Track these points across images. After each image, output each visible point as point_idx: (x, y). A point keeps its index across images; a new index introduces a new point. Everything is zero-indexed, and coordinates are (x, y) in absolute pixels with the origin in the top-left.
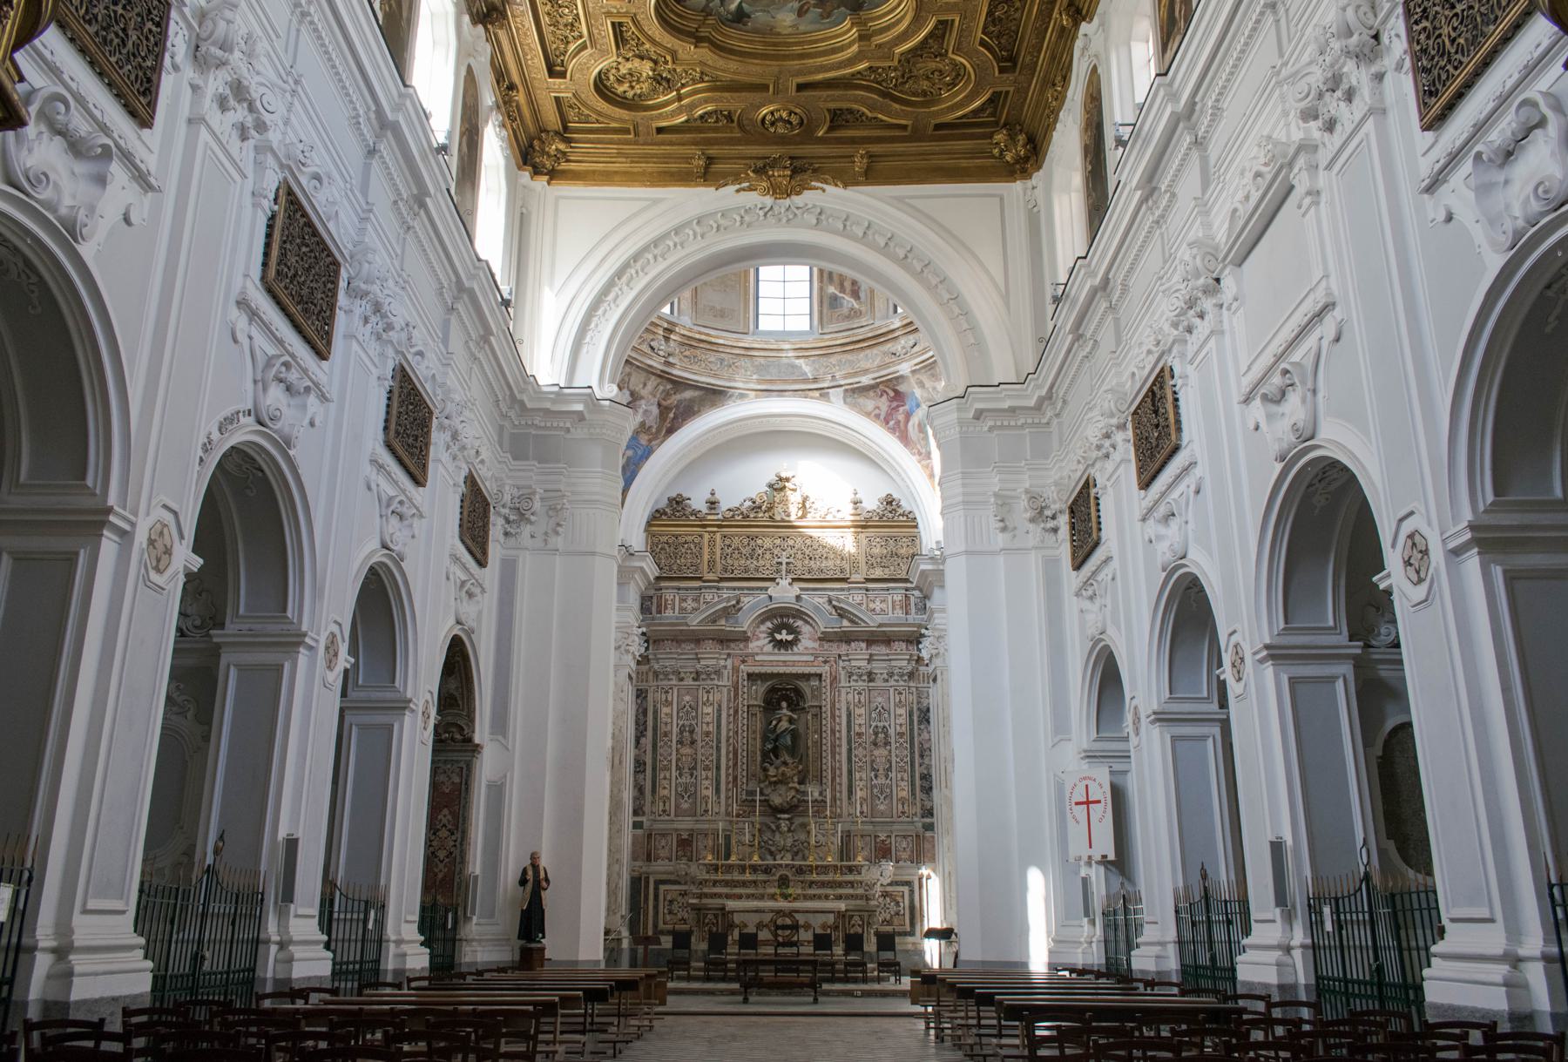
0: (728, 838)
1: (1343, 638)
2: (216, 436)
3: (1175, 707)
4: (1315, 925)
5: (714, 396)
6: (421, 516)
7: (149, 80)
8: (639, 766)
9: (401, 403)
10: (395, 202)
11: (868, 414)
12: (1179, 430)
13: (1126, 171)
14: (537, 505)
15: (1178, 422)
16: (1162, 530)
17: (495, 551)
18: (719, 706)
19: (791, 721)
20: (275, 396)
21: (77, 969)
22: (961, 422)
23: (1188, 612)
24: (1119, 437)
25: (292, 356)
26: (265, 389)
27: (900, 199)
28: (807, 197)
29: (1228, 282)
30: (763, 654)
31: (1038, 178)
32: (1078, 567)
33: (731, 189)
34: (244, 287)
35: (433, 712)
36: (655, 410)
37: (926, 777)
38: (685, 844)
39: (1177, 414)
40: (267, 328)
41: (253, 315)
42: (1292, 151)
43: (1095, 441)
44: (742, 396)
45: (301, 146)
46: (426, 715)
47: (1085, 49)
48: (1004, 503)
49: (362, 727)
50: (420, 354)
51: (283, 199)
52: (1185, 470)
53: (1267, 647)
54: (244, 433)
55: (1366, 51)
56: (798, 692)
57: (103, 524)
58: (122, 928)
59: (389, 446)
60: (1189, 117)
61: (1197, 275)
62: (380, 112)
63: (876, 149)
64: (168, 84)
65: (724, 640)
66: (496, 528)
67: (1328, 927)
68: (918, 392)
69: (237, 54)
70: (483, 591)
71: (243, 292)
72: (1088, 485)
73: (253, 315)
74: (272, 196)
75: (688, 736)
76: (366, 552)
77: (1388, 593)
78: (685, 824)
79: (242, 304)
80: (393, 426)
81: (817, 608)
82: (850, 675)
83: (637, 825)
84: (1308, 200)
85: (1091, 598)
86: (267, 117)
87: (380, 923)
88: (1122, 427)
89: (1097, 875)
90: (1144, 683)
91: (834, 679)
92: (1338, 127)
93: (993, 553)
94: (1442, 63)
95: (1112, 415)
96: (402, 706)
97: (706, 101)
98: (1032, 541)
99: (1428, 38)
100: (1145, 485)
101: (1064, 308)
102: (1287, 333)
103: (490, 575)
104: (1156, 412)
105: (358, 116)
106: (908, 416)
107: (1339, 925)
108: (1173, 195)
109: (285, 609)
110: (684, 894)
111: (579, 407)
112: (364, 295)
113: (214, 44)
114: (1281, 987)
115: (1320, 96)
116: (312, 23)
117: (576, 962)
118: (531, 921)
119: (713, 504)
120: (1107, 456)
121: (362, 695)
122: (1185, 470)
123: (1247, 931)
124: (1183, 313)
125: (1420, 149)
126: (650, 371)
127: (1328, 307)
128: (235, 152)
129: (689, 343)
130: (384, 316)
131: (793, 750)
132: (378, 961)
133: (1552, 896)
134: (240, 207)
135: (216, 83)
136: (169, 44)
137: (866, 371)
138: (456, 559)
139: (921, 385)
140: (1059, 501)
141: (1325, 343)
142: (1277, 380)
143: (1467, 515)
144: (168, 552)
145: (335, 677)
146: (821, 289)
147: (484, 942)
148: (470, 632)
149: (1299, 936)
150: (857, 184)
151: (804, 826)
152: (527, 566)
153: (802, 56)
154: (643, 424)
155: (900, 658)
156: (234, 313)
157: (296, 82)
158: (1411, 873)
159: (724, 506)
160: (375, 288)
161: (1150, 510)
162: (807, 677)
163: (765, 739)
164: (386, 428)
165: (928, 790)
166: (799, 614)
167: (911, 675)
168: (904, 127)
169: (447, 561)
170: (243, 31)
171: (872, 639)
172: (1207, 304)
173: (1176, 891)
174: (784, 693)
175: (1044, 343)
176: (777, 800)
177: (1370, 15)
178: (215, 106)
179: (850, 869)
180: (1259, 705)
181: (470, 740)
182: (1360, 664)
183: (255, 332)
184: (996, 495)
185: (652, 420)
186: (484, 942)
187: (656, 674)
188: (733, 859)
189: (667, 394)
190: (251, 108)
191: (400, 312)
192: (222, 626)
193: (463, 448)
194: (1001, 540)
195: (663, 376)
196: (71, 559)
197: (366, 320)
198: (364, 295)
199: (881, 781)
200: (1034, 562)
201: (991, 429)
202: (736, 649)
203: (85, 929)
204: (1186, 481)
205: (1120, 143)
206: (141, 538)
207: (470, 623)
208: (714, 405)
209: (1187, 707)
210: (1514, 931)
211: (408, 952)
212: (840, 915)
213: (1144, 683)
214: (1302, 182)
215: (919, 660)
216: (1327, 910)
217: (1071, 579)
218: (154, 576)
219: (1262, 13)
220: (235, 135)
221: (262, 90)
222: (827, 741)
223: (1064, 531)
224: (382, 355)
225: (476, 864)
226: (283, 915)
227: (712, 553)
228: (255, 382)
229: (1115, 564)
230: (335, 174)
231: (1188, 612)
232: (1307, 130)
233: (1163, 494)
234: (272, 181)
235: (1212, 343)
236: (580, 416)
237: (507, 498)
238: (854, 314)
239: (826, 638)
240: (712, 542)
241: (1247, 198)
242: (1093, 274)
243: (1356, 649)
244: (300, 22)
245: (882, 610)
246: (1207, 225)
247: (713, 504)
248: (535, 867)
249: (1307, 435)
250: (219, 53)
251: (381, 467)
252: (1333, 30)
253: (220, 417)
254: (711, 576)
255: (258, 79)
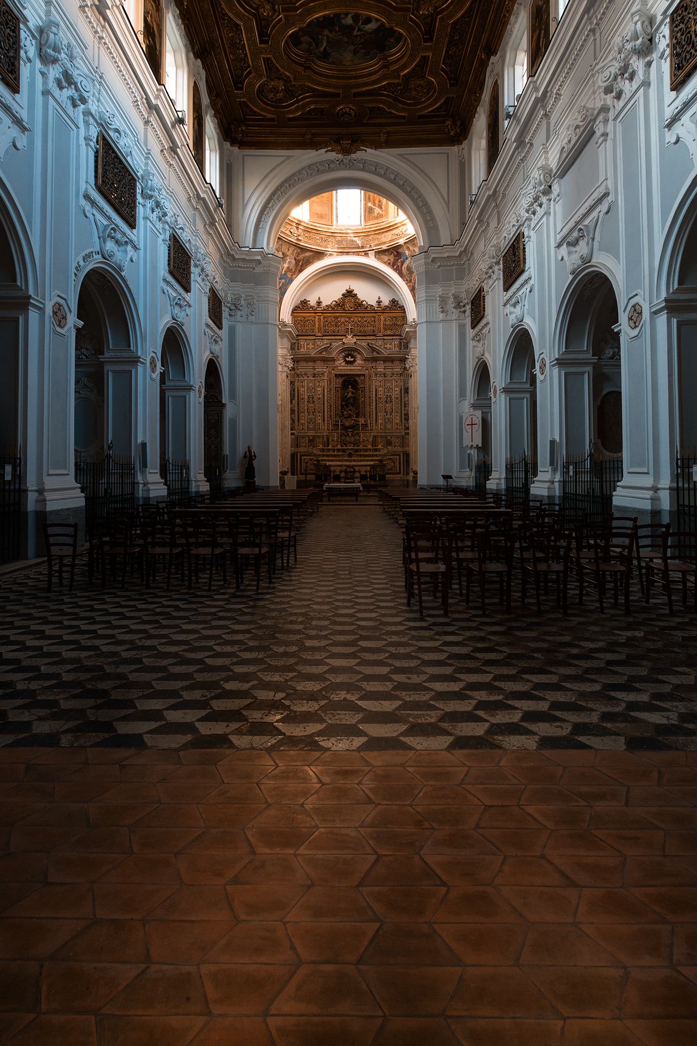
0: (328, 439)
1: (590, 356)
2: (82, 263)
3: (512, 386)
4: (565, 473)
5: (319, 255)
6: (190, 306)
7: (13, 65)
8: (292, 411)
9: (175, 253)
10: (162, 151)
11: (385, 263)
12: (525, 262)
13: (509, 130)
14: (243, 302)
15: (524, 259)
16: (512, 309)
17: (225, 323)
18: (322, 387)
19: (353, 393)
20: (110, 245)
21: (48, 498)
22: (426, 264)
23: (521, 344)
24: (496, 268)
25: (117, 225)
26: (105, 242)
27: (400, 155)
28: (359, 155)
29: (556, 188)
30: (341, 366)
31: (465, 144)
32: (473, 327)
33: (324, 150)
34: (86, 188)
35: (203, 391)
36: (293, 261)
37: (407, 415)
38: (312, 441)
39: (524, 255)
40: (101, 210)
41: (93, 203)
42: (596, 112)
43: (484, 270)
44: (331, 255)
45: (108, 114)
46: (200, 391)
47: (492, 71)
48: (443, 300)
49: (173, 397)
50: (181, 228)
51: (101, 142)
52: (526, 281)
53: (556, 359)
54: (95, 262)
55: (644, 49)
56: (356, 382)
57: (29, 304)
58: (70, 480)
59: (171, 272)
60: (543, 101)
61: (541, 184)
62: (148, 99)
63: (390, 129)
64: (25, 71)
65: (325, 360)
66: (225, 313)
67: (571, 474)
68: (407, 252)
69: (63, 56)
70: (222, 340)
71: (86, 190)
72: (481, 290)
73: (93, 203)
74: (95, 140)
75: (311, 399)
76: (165, 321)
77: (618, 333)
78: (312, 433)
79: (87, 197)
80: (172, 263)
81: (363, 347)
82: (376, 374)
83: (292, 434)
84: (602, 139)
85: (478, 341)
86: (85, 95)
87: (188, 474)
88: (498, 263)
89: (474, 452)
90: (499, 377)
91: (370, 376)
92: (623, 95)
93: (438, 322)
94: (688, 49)
95: (494, 258)
96: (189, 388)
97: (311, 103)
98: (454, 317)
99: (682, 35)
100: (506, 289)
101: (474, 207)
102: (583, 210)
103: (224, 333)
104: (514, 255)
105: (137, 101)
106: (403, 263)
107: (576, 473)
108: (532, 144)
109: (130, 346)
110: (311, 460)
111: (259, 258)
112: (151, 197)
113: (49, 47)
114: (548, 497)
115: (615, 78)
116: (105, 43)
117: (268, 487)
118: (249, 471)
119: (319, 303)
120: (490, 277)
121: (172, 384)
122: (526, 281)
123: (536, 475)
124: (532, 204)
125: (667, 101)
126: (290, 244)
127: (606, 195)
128: (71, 115)
129: (308, 230)
130: (162, 208)
131: (352, 405)
132: (188, 488)
133: (677, 463)
134: (78, 146)
135: (54, 72)
136: (22, 44)
137: (384, 243)
138: (208, 325)
139: (408, 249)
140: (466, 299)
141: (602, 214)
142: (575, 234)
143: (664, 295)
144: (65, 318)
145: (156, 376)
146: (365, 204)
147: (232, 479)
148: (217, 357)
149: (558, 477)
150: (381, 147)
151: (358, 434)
152: (240, 329)
153: (356, 77)
154: (288, 268)
155: (398, 369)
156: (83, 202)
157: (101, 77)
158: (608, 453)
159: (324, 304)
160: (156, 194)
161: (508, 301)
162: (359, 375)
163: (342, 401)
164: (169, 264)
165: (407, 420)
166: (356, 350)
167: (401, 374)
168: (404, 117)
169: (204, 327)
170: (65, 42)
171: (385, 360)
172: (544, 199)
173: (506, 459)
174: (350, 382)
175: (463, 224)
176: (347, 424)
177: (649, 27)
178: (55, 85)
179: (376, 450)
180: (550, 386)
181: (221, 402)
182: (596, 367)
183: (95, 212)
184: (440, 296)
185: (292, 266)
186: (232, 479)
187: (298, 375)
188: (330, 447)
189: (298, 254)
190: (77, 89)
191: (169, 207)
192: (103, 354)
193: (207, 275)
194: (441, 316)
195: (296, 246)
196: (17, 321)
197: (153, 212)
198: (151, 197)
199: (389, 416)
200: (454, 326)
201: (439, 267)
202: (330, 364)
203: (49, 483)
204: (526, 287)
205: (509, 116)
206: (49, 311)
207: (217, 352)
208: (319, 259)
209: (517, 386)
210: (657, 477)
211: (199, 483)
212: (373, 466)
213: (499, 377)
214: (599, 129)
215: (405, 368)
216: (571, 467)
217: (470, 333)
218: (58, 329)
219: (588, 35)
220: (69, 103)
221: (81, 78)
222: (367, 400)
223: (468, 312)
224: (163, 229)
225: (227, 450)
226: (143, 473)
227: (320, 324)
228: (99, 238)
229: (490, 326)
230: (128, 131)
231: (521, 344)
232: (605, 100)
233: (514, 293)
234: (94, 132)
235: (545, 219)
236: (259, 262)
237: (229, 299)
238: (380, 216)
239: (366, 360)
240: (319, 319)
241: (570, 141)
242: (489, 189)
243: (595, 360)
244: (99, 43)
245: (390, 347)
246: (547, 159)
247: (319, 303)
248: (250, 452)
249: (586, 260)
250: (52, 53)
251: (168, 283)
252: (628, 38)
253: (83, 254)
254: (319, 334)
255: (77, 72)
